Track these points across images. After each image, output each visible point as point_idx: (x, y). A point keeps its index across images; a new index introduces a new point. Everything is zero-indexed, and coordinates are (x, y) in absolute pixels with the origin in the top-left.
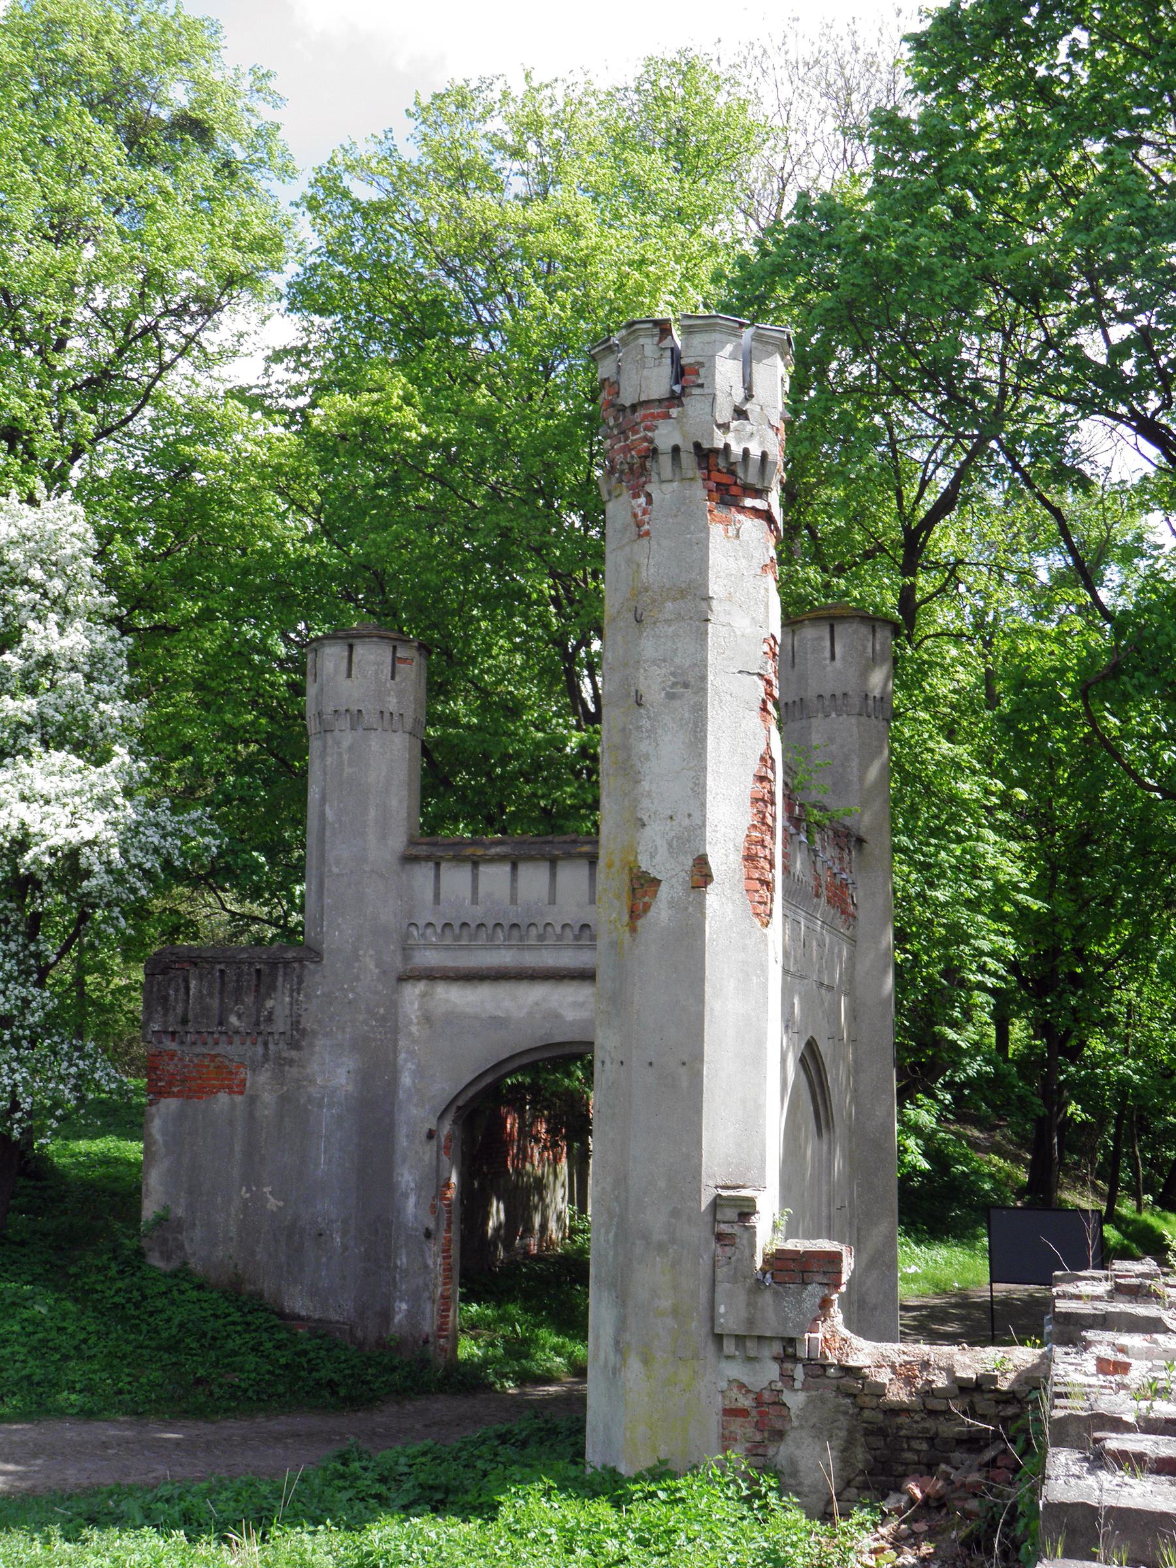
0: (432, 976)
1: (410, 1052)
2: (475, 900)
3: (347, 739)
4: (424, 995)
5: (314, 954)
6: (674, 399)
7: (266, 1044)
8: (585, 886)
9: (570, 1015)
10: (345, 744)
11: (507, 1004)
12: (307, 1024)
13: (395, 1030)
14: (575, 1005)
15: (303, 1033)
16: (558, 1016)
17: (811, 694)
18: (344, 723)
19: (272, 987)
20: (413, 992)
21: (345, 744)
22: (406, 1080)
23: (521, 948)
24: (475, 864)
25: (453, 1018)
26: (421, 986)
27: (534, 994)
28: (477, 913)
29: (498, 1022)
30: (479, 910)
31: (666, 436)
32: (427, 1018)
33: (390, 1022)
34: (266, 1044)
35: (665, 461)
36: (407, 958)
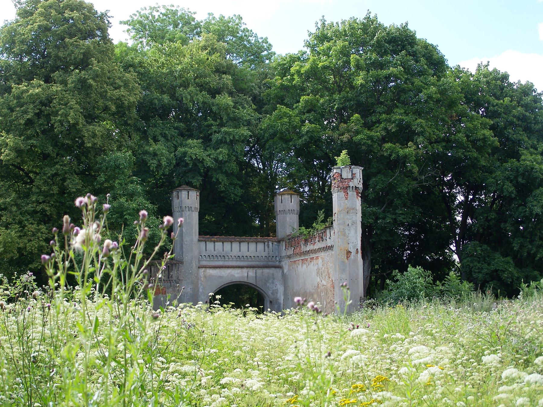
0: (206, 267)
1: (201, 284)
2: (215, 250)
3: (188, 213)
4: (204, 271)
5: (182, 262)
6: (352, 179)
7: (171, 283)
8: (238, 248)
9: (237, 275)
10: (187, 214)
11: (223, 273)
12: (180, 278)
13: (198, 279)
14: (237, 273)
15: (180, 280)
16: (234, 276)
17: (287, 209)
18: (187, 209)
19: (172, 270)
20: (202, 270)
21: (187, 214)
22: (201, 290)
23: (225, 261)
24: (214, 242)
25: (211, 276)
26: (203, 269)
27: (228, 271)
28: (215, 253)
29: (221, 277)
30: (215, 252)
31: (351, 184)
32: (205, 276)
33: (198, 278)
34: (171, 283)
35: (351, 188)
36: (199, 263)
